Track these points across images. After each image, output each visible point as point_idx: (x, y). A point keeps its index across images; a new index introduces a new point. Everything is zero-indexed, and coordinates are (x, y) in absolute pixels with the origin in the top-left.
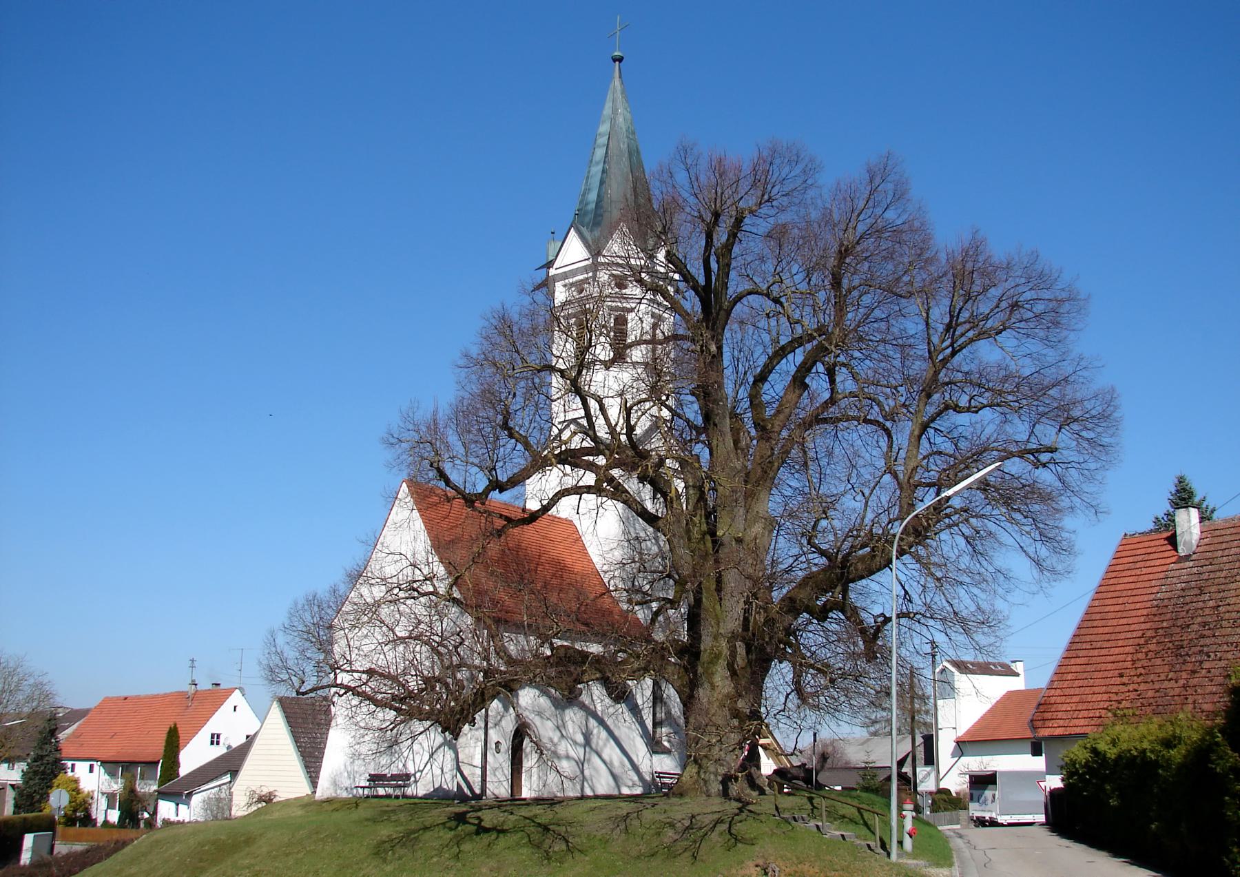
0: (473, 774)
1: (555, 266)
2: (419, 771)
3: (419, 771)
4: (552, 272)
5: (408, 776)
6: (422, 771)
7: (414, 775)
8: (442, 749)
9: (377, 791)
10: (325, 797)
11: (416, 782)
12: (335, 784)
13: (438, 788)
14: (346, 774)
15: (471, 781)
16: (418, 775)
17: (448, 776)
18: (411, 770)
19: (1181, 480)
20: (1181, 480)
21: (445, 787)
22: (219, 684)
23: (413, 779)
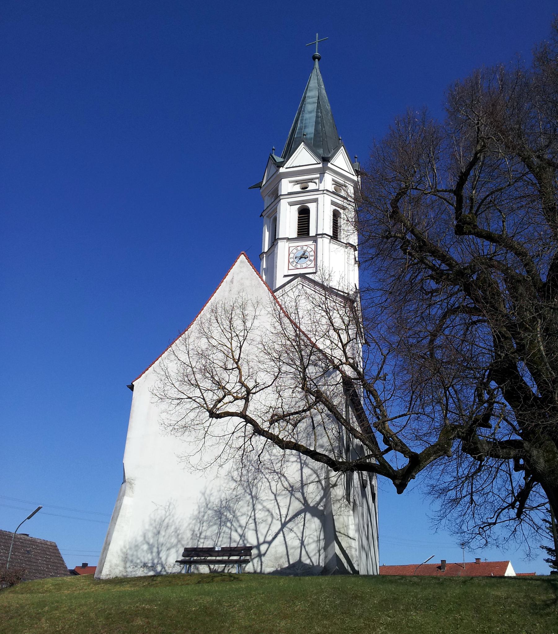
0: (350, 547)
1: (285, 166)
2: (265, 542)
3: (265, 542)
4: (282, 170)
5: (247, 550)
6: (270, 543)
7: (258, 547)
8: (303, 515)
9: (197, 569)
10: (112, 576)
11: (260, 555)
12: (125, 560)
13: (294, 565)
14: (145, 547)
15: (349, 555)
16: (263, 548)
17: (312, 548)
18: (252, 540)
19: (400, 492)
20: (400, 492)
21: (308, 562)
22: (28, 535)
23: (254, 552)
